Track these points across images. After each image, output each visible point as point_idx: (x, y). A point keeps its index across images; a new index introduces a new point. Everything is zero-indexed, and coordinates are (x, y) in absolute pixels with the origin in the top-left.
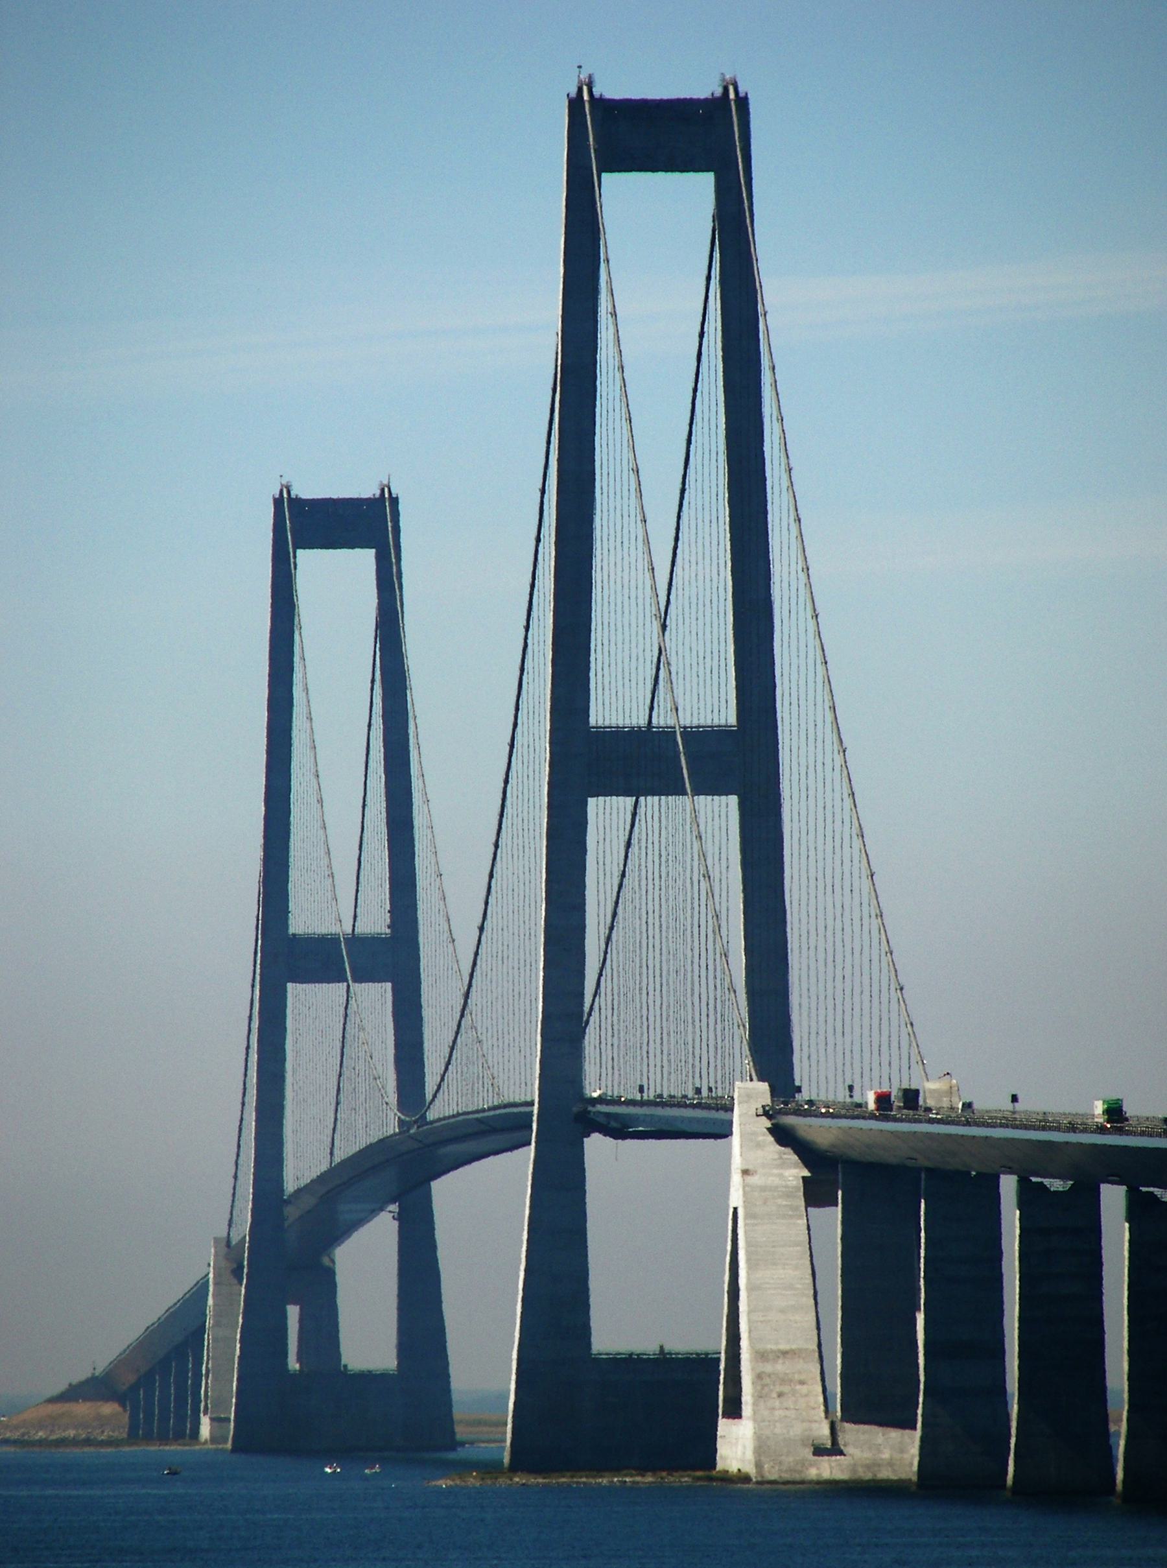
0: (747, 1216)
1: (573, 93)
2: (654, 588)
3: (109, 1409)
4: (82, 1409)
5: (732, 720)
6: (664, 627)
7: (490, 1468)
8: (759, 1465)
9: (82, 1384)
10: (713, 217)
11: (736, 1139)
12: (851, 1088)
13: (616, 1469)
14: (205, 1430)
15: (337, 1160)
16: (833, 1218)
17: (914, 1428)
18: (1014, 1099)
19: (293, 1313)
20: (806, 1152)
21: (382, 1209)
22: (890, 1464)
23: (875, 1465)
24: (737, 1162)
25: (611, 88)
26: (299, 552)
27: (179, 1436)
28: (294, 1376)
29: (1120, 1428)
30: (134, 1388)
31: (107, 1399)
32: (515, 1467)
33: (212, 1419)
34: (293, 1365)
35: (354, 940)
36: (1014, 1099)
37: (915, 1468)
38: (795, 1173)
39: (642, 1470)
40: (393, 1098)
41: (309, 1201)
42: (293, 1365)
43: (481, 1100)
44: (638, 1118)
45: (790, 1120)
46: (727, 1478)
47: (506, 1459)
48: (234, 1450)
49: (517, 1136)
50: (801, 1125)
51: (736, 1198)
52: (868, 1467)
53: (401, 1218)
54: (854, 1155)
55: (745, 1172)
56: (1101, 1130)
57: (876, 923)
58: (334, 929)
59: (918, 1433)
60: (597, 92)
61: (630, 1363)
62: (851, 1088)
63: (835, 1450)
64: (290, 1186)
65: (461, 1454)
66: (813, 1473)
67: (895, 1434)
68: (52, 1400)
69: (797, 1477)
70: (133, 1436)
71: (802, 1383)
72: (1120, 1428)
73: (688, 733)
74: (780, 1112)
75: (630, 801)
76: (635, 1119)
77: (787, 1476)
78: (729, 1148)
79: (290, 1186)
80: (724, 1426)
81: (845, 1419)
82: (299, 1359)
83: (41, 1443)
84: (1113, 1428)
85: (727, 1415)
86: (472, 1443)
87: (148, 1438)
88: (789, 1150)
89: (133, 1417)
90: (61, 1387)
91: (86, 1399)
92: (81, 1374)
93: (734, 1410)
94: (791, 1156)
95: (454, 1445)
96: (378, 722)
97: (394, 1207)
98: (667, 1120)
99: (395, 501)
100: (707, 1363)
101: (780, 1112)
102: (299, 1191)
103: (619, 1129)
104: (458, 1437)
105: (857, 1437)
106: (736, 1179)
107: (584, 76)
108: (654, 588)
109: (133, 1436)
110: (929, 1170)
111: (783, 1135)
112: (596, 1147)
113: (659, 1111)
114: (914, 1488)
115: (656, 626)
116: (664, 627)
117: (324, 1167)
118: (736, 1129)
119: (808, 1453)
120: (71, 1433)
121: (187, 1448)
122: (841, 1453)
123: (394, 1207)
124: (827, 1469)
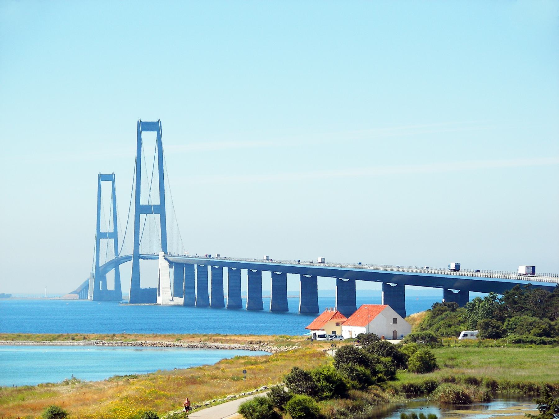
1: (138, 121)
2: (149, 186)
3: (76, 295)
7: (126, 303)
8: (162, 303)
9: (73, 292)
14: (89, 298)
15: (107, 262)
16: (172, 270)
17: (183, 298)
18: (196, 254)
19: (101, 282)
20: (169, 261)
22: (180, 302)
23: (178, 302)
27: (85, 299)
28: (101, 291)
29: (210, 301)
30: (80, 292)
31: (76, 294)
32: (130, 303)
33: (90, 296)
34: (101, 289)
35: (109, 233)
36: (196, 254)
37: (183, 303)
39: (147, 303)
40: (114, 254)
41: (103, 268)
42: (101, 289)
44: (191, 384)
45: (166, 257)
47: (129, 302)
48: (93, 301)
49: (131, 259)
50: (168, 258)
51: (160, 267)
53: (115, 270)
54: (175, 262)
57: (179, 236)
58: (106, 232)
59: (173, 269)
61: (146, 289)
63: (173, 301)
64: (100, 266)
67: (180, 298)
68: (69, 294)
69: (168, 304)
70: (79, 299)
72: (210, 301)
74: (166, 256)
75: (146, 214)
77: (166, 304)
79: (100, 266)
80: (158, 298)
81: (174, 297)
83: (67, 299)
84: (209, 298)
85: (158, 296)
87: (82, 299)
89: (80, 296)
93: (159, 295)
95: (122, 300)
96: (112, 204)
97: (114, 269)
98: (150, 257)
99: (114, 175)
101: (166, 256)
102: (101, 266)
103: (144, 258)
104: (123, 299)
105: (175, 299)
107: (140, 119)
108: (149, 186)
109: (79, 299)
110: (185, 264)
111: (166, 259)
112: (141, 260)
113: (149, 256)
114: (183, 306)
116: (150, 192)
117: (105, 263)
122: (173, 301)
123: (114, 269)
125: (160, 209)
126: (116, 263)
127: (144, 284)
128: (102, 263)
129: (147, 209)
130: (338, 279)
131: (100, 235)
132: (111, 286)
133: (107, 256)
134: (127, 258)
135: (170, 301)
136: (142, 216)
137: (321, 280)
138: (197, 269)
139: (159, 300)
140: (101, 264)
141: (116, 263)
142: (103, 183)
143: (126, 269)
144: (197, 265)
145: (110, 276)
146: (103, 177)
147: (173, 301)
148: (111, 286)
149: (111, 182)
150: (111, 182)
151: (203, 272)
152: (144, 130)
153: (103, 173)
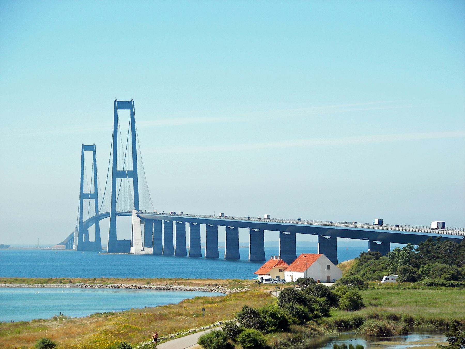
0: (134, 225)
1: (115, 101)
2: (124, 155)
4: (61, 246)
5: (132, 170)
6: (125, 160)
7: (105, 252)
8: (135, 252)
10: (7, 246)
11: (133, 216)
12: (145, 211)
13: (119, 252)
14: (74, 248)
15: (89, 218)
16: (143, 225)
17: (152, 248)
18: (163, 212)
19: (84, 235)
21: (93, 224)
24: (133, 219)
25: (85, 144)
26: (118, 110)
27: (71, 249)
29: (175, 248)
30: (66, 243)
31: (63, 245)
33: (75, 247)
34: (84, 241)
35: (90, 194)
36: (163, 212)
38: (139, 220)
41: (85, 223)
42: (84, 241)
43: (105, 212)
45: (138, 214)
46: (132, 253)
47: (107, 252)
48: (77, 250)
49: (109, 216)
51: (133, 223)
52: (147, 252)
53: (96, 225)
54: (146, 218)
55: (134, 220)
56: (170, 215)
60: (84, 145)
61: (121, 241)
62: (145, 211)
63: (144, 250)
65: (102, 251)
66: (141, 253)
67: (150, 249)
68: (58, 245)
69: (139, 253)
70: (66, 249)
71: (140, 243)
72: (175, 248)
73: (128, 171)
74: (138, 213)
75: (121, 179)
76: (121, 214)
78: (132, 217)
79: (83, 221)
80: (131, 248)
81: (145, 247)
82: (85, 240)
84: (174, 248)
86: (103, 250)
87: (68, 249)
88: (139, 217)
89: (66, 247)
90: (58, 243)
91: (61, 245)
92: (60, 242)
93: (133, 246)
94: (139, 218)
95: (102, 250)
96: (93, 170)
97: (95, 224)
98: (125, 214)
99: (134, 102)
100: (130, 241)
101: (138, 213)
102: (84, 222)
103: (120, 215)
104: (102, 249)
106: (133, 220)
107: (116, 99)
108: (124, 155)
109: (66, 249)
110: (154, 220)
111: (138, 216)
112: (117, 216)
114: (152, 255)
115: (124, 159)
117: (87, 219)
118: (133, 215)
119: (141, 250)
120: (59, 248)
121: (69, 250)
122: (144, 251)
123: (95, 224)
124: (143, 252)
125: (133, 174)
126: (96, 219)
127: (120, 237)
128: (85, 219)
129: (122, 174)
130: (281, 232)
131: (83, 196)
132: (92, 238)
133: (89, 213)
134: (106, 215)
135: (142, 250)
136: (118, 180)
137: (267, 233)
138: (164, 224)
139: (133, 250)
140: (84, 220)
141: (96, 219)
142: (120, 112)
143: (105, 224)
144: (164, 221)
145: (92, 229)
146: (86, 148)
147: (144, 251)
148: (92, 238)
149: (92, 151)
150: (92, 151)
151: (169, 227)
152: (120, 108)
153: (86, 144)
